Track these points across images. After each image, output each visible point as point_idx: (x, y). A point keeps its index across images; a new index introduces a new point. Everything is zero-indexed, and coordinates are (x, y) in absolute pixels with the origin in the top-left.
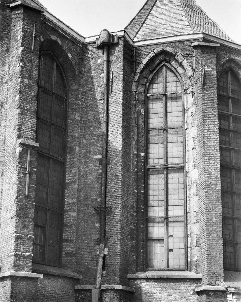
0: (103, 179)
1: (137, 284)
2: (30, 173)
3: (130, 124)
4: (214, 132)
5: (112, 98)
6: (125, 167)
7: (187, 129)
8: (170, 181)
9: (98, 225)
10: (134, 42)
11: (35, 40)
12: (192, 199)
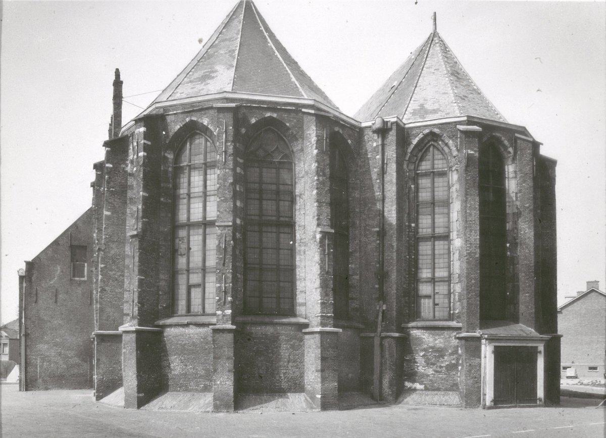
1: (409, 331)
2: (328, 254)
5: (387, 178)
6: (399, 239)
10: (405, 124)
11: (326, 142)
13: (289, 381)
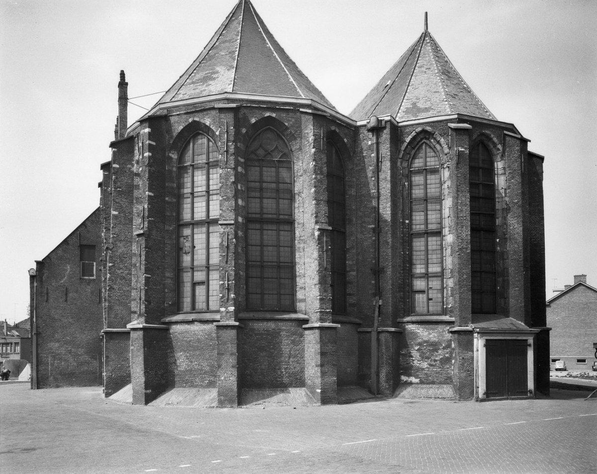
0: (377, 245)
2: (327, 251)
3: (396, 197)
4: (466, 205)
5: (382, 176)
7: (444, 199)
8: (430, 243)
9: (373, 282)
10: (398, 123)
12: (447, 258)
13: (290, 376)
